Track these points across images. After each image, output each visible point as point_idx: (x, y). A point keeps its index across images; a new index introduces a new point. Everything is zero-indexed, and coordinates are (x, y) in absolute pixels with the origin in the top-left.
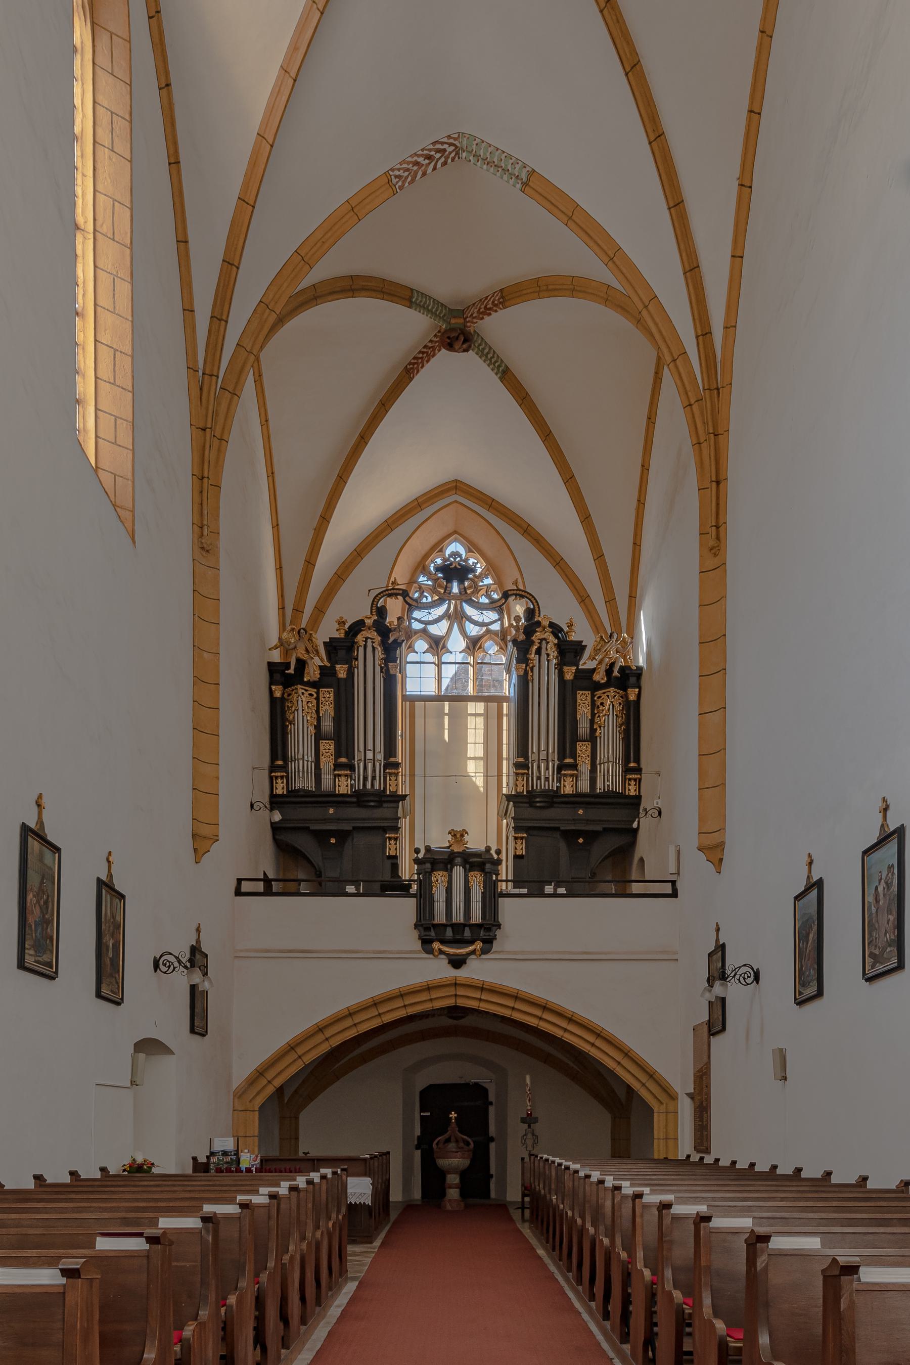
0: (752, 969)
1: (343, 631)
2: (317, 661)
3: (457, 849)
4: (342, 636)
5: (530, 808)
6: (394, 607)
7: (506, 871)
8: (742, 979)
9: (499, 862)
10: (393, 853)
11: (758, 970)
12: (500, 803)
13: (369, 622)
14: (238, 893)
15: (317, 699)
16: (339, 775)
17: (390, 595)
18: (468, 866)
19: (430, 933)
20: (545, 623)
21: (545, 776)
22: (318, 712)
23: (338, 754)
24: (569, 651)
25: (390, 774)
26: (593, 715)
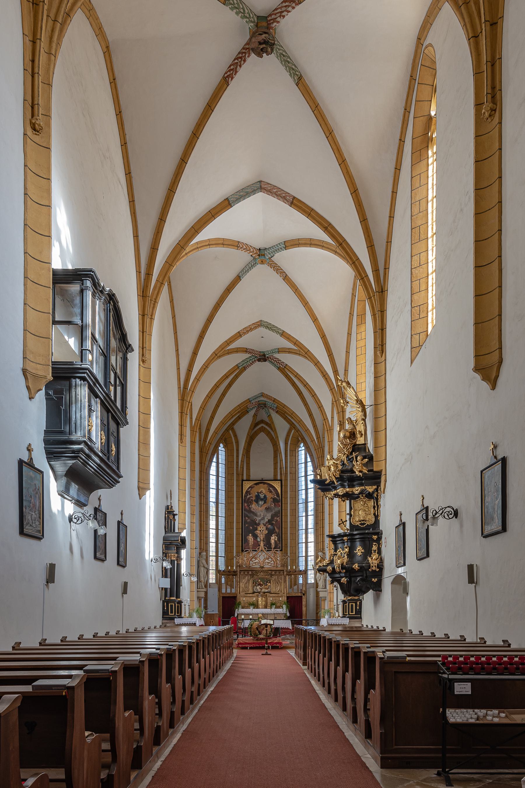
0: (453, 509)
8: (446, 515)
11: (457, 510)
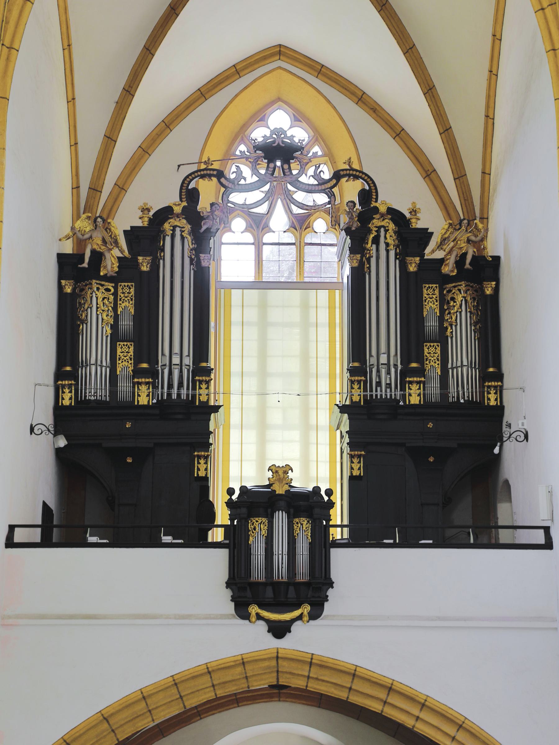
1: (146, 219)
2: (116, 253)
3: (280, 490)
4: (146, 224)
5: (369, 423)
6: (207, 190)
7: (339, 514)
9: (331, 504)
10: (202, 474)
12: (331, 413)
13: (177, 210)
14: (10, 543)
15: (115, 294)
16: (139, 383)
17: (202, 177)
18: (292, 511)
19: (249, 592)
20: (383, 209)
21: (385, 381)
22: (115, 309)
23: (138, 359)
24: (411, 238)
25: (201, 382)
26: (442, 311)
